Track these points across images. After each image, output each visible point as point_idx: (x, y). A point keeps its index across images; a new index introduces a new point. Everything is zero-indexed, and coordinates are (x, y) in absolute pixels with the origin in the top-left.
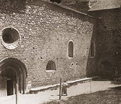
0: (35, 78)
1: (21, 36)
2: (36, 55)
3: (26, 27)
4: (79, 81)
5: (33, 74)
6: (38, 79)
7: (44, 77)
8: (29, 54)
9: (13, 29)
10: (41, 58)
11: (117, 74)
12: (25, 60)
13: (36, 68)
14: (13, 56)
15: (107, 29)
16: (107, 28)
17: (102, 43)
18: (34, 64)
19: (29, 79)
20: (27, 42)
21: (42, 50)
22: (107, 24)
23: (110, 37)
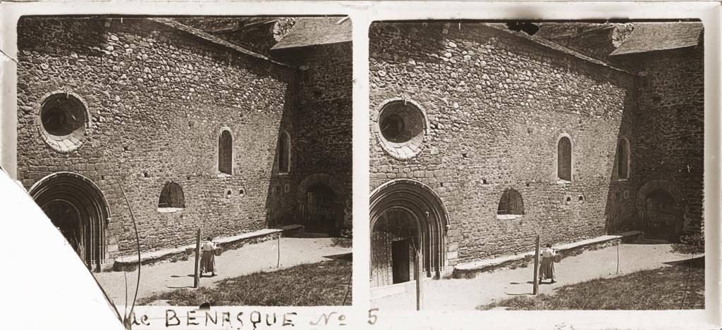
4: (581, 244)
6: (477, 238)
11: (690, 225)
14: (408, 178)
15: (663, 104)
16: (662, 102)
17: (648, 141)
22: (323, 83)
23: (669, 126)
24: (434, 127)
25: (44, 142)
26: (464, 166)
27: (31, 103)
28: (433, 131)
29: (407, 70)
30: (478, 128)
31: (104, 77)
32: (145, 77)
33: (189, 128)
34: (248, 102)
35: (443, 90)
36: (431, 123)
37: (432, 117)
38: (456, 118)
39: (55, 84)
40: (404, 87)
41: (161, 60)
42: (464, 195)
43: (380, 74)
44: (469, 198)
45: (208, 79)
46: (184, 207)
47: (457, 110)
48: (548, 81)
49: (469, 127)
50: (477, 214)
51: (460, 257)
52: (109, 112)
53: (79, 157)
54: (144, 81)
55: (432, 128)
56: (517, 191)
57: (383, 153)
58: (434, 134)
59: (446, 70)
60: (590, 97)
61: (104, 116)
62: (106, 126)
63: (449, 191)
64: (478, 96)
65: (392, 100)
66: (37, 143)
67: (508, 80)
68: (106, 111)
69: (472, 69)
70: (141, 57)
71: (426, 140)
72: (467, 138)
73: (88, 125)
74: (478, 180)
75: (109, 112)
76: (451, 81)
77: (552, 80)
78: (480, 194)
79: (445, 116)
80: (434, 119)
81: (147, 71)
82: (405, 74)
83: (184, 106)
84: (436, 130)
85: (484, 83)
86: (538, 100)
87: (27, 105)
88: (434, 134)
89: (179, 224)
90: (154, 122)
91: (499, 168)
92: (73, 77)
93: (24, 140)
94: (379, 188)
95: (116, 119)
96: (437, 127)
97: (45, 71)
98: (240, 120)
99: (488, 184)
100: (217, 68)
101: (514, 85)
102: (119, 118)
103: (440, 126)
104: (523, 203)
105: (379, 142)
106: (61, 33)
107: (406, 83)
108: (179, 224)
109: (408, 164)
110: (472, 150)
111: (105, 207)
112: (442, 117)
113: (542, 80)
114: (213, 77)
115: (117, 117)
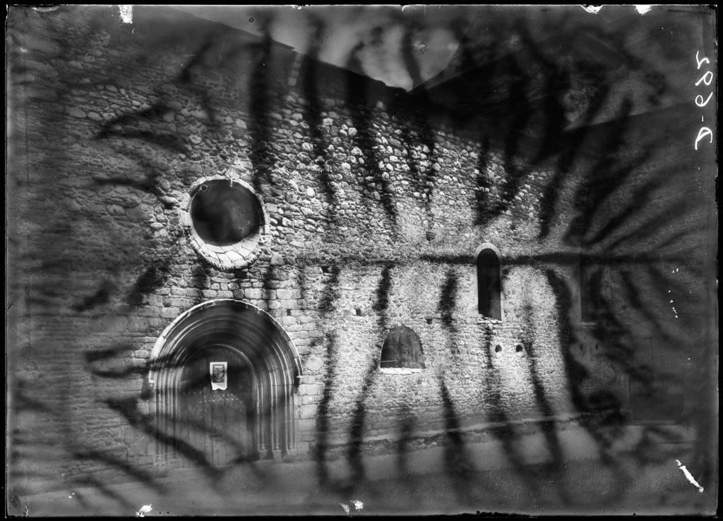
20: (294, 243)
24: (276, 222)
25: (196, 251)
27: (175, 192)
28: (275, 228)
29: (233, 135)
30: (346, 228)
31: (288, 159)
32: (354, 161)
33: (427, 242)
34: (523, 207)
35: (290, 169)
36: (272, 216)
38: (310, 211)
39: (211, 166)
40: (229, 161)
41: (379, 137)
43: (194, 141)
45: (455, 169)
46: (423, 366)
47: (313, 200)
48: (457, 162)
52: (296, 211)
53: (251, 278)
54: (352, 168)
55: (272, 224)
56: (412, 330)
57: (196, 258)
58: (277, 233)
59: (295, 138)
60: (527, 189)
61: (289, 217)
62: (293, 232)
63: (301, 323)
64: (344, 179)
65: (210, 178)
66: (185, 253)
67: (393, 158)
68: (292, 210)
69: (335, 139)
70: (347, 131)
71: (263, 241)
72: (330, 242)
73: (264, 230)
74: (347, 308)
75: (296, 211)
76: (301, 155)
77: (464, 161)
78: (350, 330)
79: (293, 207)
80: (275, 210)
81: (356, 153)
82: (231, 142)
83: (418, 209)
84: (280, 228)
85: (354, 161)
86: (441, 189)
87: (168, 195)
88: (277, 233)
89: (416, 394)
90: (370, 231)
92: (239, 156)
93: (164, 246)
94: (190, 310)
95: (309, 223)
96: (280, 223)
97: (197, 147)
98: (510, 235)
99: (364, 315)
100: (469, 152)
101: (403, 166)
102: (313, 221)
103: (285, 221)
104: (422, 350)
105: (190, 241)
106: (221, 91)
107: (232, 155)
108: (416, 394)
111: (294, 358)
113: (448, 160)
114: (462, 166)
115: (310, 220)
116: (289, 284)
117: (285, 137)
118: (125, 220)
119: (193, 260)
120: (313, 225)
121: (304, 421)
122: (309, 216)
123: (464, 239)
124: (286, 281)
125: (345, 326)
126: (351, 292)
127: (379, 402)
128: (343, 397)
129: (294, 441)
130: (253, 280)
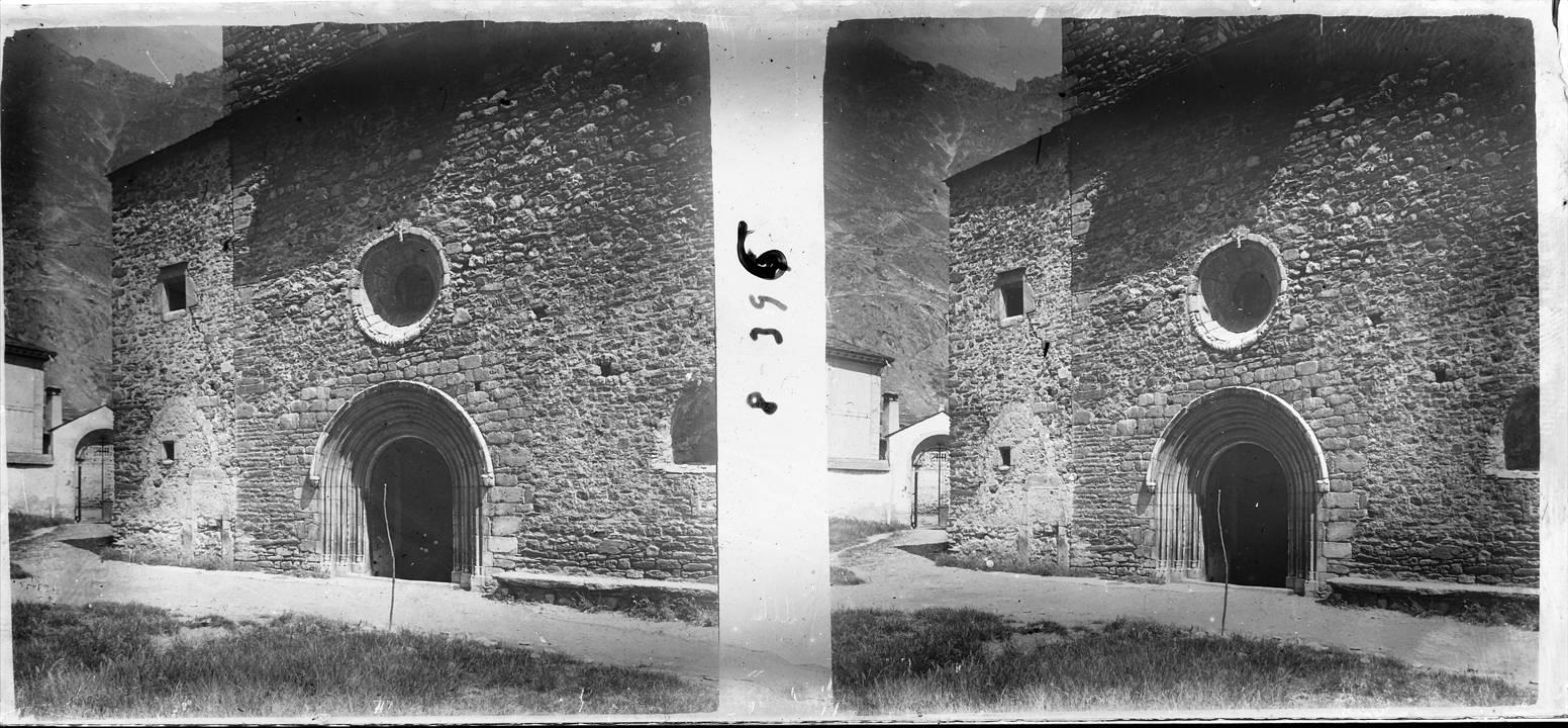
0: (548, 509)
1: (1290, 267)
2: (560, 351)
3: (489, 200)
4: (709, 585)
5: (535, 480)
6: (576, 514)
7: (1469, 517)
8: (1337, 360)
9: (1246, 242)
10: (607, 370)
12: (476, 394)
13: (1390, 445)
14: (1242, 384)
18: (1376, 420)
19: (501, 509)
20: (488, 287)
21: (618, 311)
26: (536, 338)
37: (1292, 255)
42: (1373, 413)
44: (1388, 421)
49: (1391, 247)
50: (578, 455)
51: (1358, 559)
55: (455, 270)
75: (1328, 246)
91: (661, 325)
109: (1244, 358)
110: (1399, 299)
112: (1516, 253)
116: (479, 346)
117: (477, 139)
118: (1138, 323)
119: (360, 342)
120: (521, 250)
121: (498, 540)
122: (1351, 245)
123: (77, 115)
124: (474, 344)
125: (575, 395)
126: (1425, 345)
127: (1481, 526)
128: (1402, 514)
129: (481, 565)
130: (427, 351)
